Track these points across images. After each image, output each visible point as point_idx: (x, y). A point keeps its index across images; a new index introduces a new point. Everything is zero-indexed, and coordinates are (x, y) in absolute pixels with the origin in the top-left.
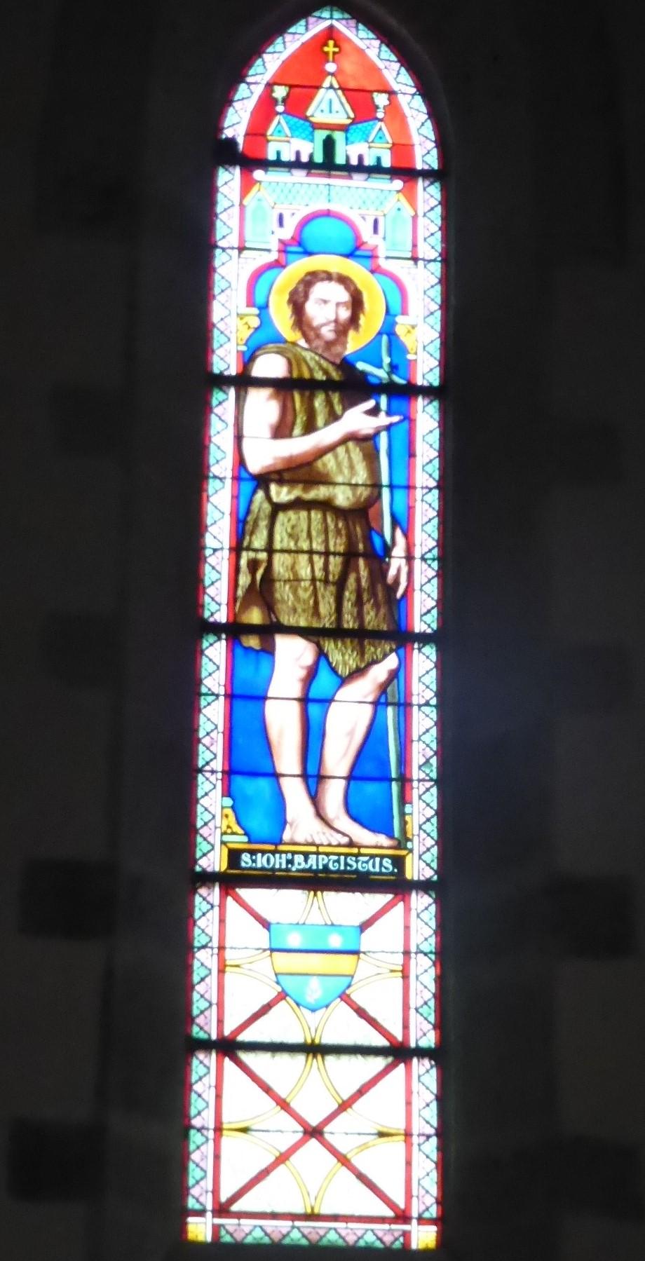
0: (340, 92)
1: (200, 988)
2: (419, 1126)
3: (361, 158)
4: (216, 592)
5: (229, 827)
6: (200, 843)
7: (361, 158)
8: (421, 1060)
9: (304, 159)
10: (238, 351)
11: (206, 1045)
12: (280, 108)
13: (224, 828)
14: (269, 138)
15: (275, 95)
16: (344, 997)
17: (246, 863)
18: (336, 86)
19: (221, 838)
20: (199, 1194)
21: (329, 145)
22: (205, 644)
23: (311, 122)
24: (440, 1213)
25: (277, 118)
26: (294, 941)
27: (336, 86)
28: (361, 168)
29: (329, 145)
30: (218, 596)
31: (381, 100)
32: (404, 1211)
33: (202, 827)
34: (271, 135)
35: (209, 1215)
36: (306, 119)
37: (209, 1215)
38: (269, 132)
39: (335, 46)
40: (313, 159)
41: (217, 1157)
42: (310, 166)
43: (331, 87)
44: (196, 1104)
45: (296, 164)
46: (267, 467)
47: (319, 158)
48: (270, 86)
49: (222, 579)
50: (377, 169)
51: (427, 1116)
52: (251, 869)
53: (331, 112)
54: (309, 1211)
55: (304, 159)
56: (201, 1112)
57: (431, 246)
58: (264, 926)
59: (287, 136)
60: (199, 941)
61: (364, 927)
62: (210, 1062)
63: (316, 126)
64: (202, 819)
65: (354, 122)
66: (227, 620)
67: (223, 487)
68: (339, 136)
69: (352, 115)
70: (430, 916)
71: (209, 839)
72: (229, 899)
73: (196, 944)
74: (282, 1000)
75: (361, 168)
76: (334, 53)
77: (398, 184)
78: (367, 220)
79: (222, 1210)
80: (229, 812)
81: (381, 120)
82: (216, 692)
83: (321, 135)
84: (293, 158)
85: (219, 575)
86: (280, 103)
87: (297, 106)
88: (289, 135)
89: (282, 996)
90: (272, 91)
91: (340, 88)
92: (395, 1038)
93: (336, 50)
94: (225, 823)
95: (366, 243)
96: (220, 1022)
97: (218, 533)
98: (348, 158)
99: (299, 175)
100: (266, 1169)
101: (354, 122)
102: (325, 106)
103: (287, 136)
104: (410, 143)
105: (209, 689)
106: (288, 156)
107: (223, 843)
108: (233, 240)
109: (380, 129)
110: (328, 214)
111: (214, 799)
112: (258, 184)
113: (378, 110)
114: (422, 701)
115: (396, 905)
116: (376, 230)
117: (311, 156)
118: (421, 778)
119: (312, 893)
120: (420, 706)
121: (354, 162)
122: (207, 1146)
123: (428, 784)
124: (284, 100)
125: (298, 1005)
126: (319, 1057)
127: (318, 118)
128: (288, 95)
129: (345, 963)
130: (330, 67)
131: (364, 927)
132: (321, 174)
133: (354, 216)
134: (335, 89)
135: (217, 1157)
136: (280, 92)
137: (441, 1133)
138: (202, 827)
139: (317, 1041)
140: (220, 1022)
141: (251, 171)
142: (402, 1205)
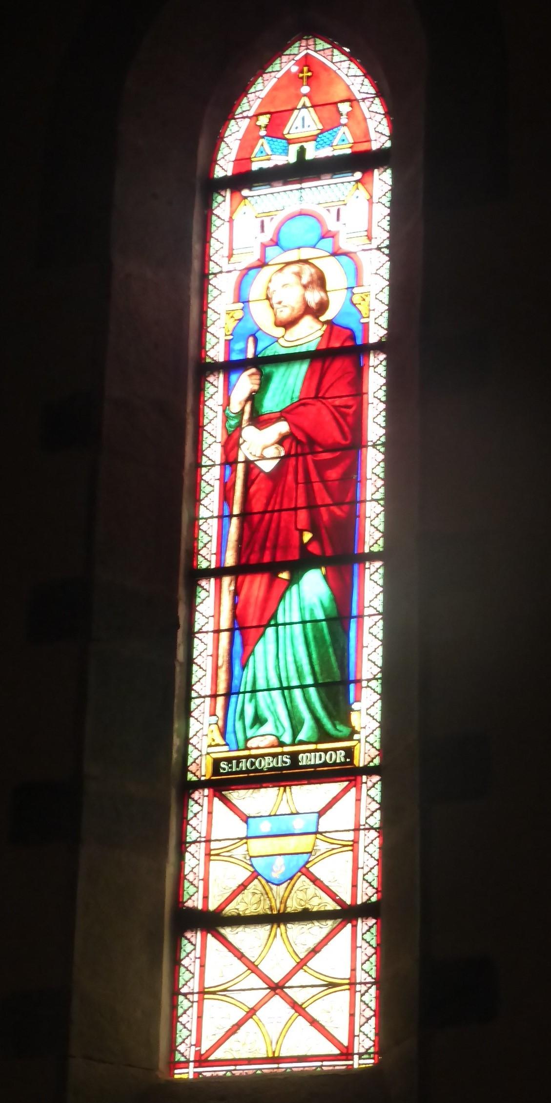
0: (311, 109)
2: (361, 976)
8: (364, 920)
10: (226, 340)
12: (263, 132)
14: (252, 159)
16: (304, 870)
17: (224, 769)
20: (186, 1050)
26: (265, 827)
27: (308, 104)
30: (189, 1023)
32: (347, 1048)
35: (192, 1065)
37: (192, 1065)
39: (309, 71)
41: (200, 1017)
43: (304, 106)
46: (252, 263)
49: (213, 540)
51: (367, 970)
52: (228, 773)
53: (303, 126)
54: (271, 1055)
56: (188, 982)
57: (382, 236)
59: (268, 155)
60: (190, 838)
61: (321, 813)
62: (210, 587)
63: (290, 142)
67: (224, 201)
70: (376, 793)
73: (188, 840)
74: (249, 1018)
76: (308, 77)
78: (331, 211)
79: (202, 1060)
81: (345, 125)
85: (220, 268)
87: (275, 129)
88: (270, 153)
89: (255, 875)
92: (345, 902)
93: (310, 74)
95: (330, 231)
96: (206, 898)
97: (213, 452)
100: (242, 884)
102: (299, 122)
103: (268, 155)
108: (194, 986)
113: (342, 117)
114: (362, 1050)
119: (275, 926)
122: (193, 1009)
125: (268, 881)
126: (282, 927)
129: (304, 843)
131: (321, 813)
132: (294, 180)
133: (320, 211)
135: (200, 1017)
136: (264, 120)
139: (282, 789)
140: (206, 898)
142: (346, 1043)
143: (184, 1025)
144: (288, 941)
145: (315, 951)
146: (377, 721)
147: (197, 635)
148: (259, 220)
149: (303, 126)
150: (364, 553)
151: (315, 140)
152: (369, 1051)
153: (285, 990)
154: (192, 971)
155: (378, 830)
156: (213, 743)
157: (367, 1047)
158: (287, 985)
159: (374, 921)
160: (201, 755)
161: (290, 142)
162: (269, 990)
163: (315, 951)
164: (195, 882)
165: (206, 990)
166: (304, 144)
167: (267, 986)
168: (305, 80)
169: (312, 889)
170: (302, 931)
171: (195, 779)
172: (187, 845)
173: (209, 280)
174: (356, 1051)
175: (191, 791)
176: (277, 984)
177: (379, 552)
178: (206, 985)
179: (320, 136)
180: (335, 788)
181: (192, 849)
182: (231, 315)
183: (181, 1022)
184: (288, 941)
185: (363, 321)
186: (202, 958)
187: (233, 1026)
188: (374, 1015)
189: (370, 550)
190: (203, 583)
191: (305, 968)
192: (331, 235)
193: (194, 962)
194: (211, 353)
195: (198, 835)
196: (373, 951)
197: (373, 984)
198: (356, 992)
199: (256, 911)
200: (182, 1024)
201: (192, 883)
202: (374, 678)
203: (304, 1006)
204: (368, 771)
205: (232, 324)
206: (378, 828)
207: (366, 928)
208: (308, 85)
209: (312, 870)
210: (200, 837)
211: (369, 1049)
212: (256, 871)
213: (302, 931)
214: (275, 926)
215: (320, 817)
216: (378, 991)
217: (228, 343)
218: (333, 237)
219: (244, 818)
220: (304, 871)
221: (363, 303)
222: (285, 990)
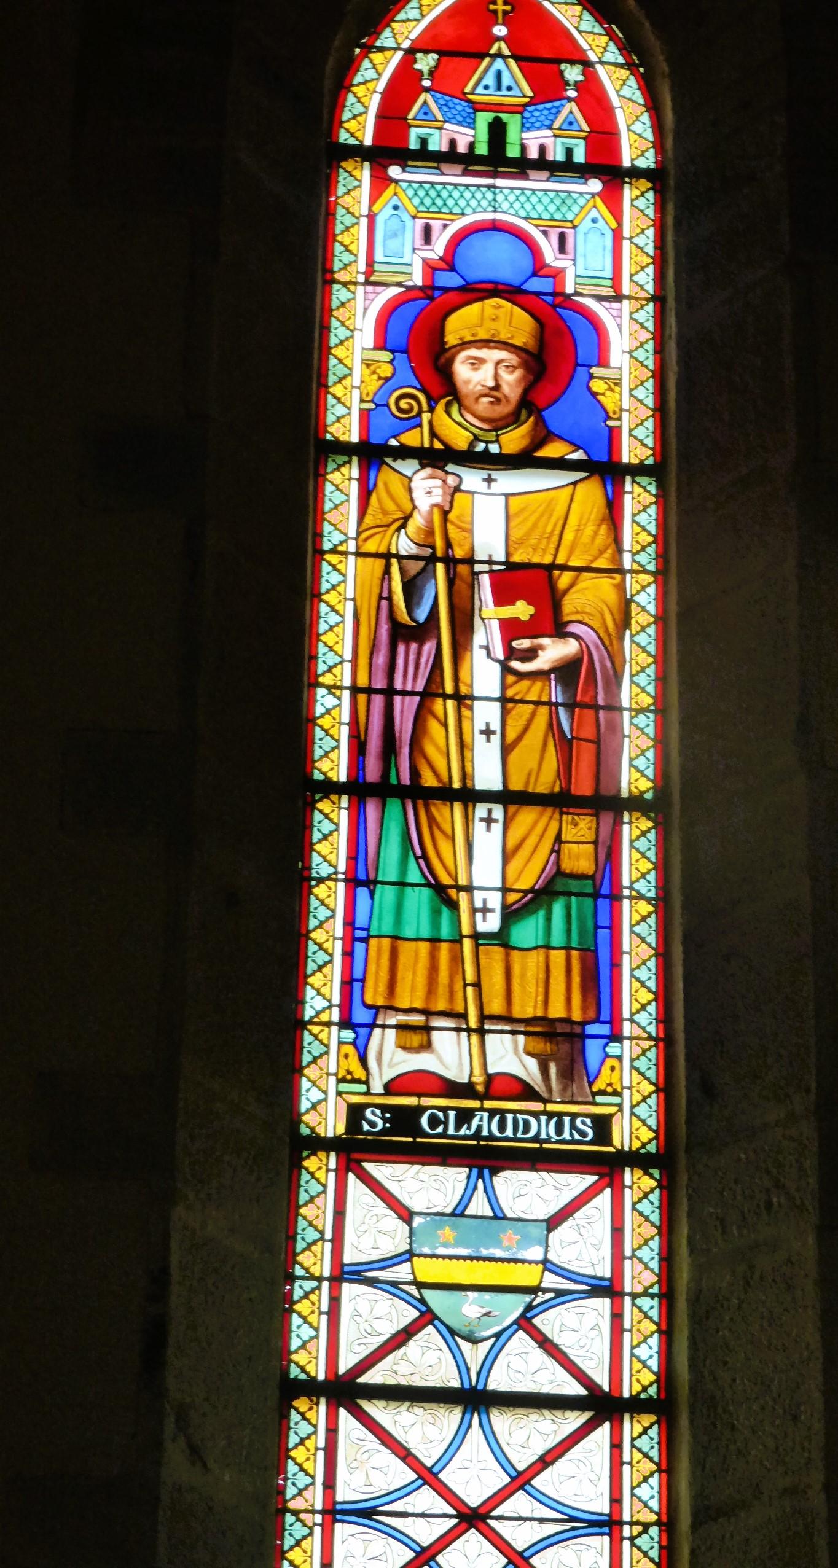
0: (511, 61)
1: (316, 980)
3: (542, 149)
4: (335, 639)
5: (349, 1072)
6: (336, 329)
7: (542, 149)
8: (635, 1415)
9: (462, 149)
10: (360, 409)
11: (311, 1388)
13: (341, 1075)
15: (417, 66)
17: (372, 1124)
18: (507, 52)
19: (337, 1087)
21: (497, 131)
22: (331, 466)
23: (469, 101)
24: (660, 610)
25: (423, 96)
28: (544, 164)
29: (497, 131)
31: (573, 73)
33: (337, 346)
34: (414, 119)
36: (463, 96)
38: (410, 116)
40: (462, 807)
42: (468, 161)
43: (499, 55)
44: (294, 1478)
45: (450, 157)
47: (482, 149)
48: (411, 52)
49: (363, 187)
50: (567, 168)
53: (499, 88)
55: (462, 149)
58: (401, 1218)
61: (554, 1222)
63: (477, 107)
64: (312, 1007)
65: (533, 102)
66: (326, 1377)
68: (513, 123)
69: (530, 94)
71: (336, 648)
72: (351, 1177)
75: (544, 164)
76: (505, 13)
77: (595, 185)
80: (350, 1049)
82: (317, 1274)
83: (484, 119)
84: (445, 148)
86: (426, 76)
88: (440, 118)
90: (415, 61)
91: (517, 58)
92: (600, 1388)
94: (344, 1064)
98: (523, 148)
99: (453, 176)
101: (533, 102)
102: (490, 80)
103: (437, 121)
104: (618, 705)
105: (307, 1270)
106: (437, 143)
107: (339, 1094)
109: (571, 112)
110: (495, 227)
111: (314, 1354)
112: (393, 185)
114: (639, 1289)
115: (601, 1191)
116: (562, 248)
117: (472, 146)
118: (634, 1035)
120: (634, 1296)
121: (533, 154)
123: (647, 1044)
124: (432, 73)
127: (480, 96)
128: (437, 66)
130: (500, 30)
131: (554, 1222)
134: (504, 57)
136: (425, 63)
137: (660, 708)
138: (337, 346)
141: (386, 167)
143: (312, 1174)
144: (491, 1438)
145: (545, 1461)
146: (649, 218)
147: (328, 557)
148: (420, 223)
149: (499, 88)
150: (621, 1398)
151: (521, 113)
152: (651, 1291)
153: (490, 1522)
154: (311, 1472)
155: (654, 902)
156: (349, 1077)
157: (647, 1284)
158: (494, 1513)
159: (653, 1418)
160: (341, 663)
161: (477, 107)
162: (455, 1521)
163: (545, 1461)
164: (313, 1319)
165: (338, 1507)
166: (500, 115)
167: (454, 1512)
168: (500, 15)
169: (538, 1356)
170: (521, 1425)
171: (352, 141)
172: (313, 883)
173: (311, 887)
174: (627, 1288)
175: (305, 1154)
176: (474, 1510)
177: (648, 169)
178: (339, 1498)
179: (529, 108)
180: (580, 1182)
181: (321, 891)
182: (372, 368)
183: (312, 986)
184: (491, 1438)
185: (610, 423)
186: (331, 1450)
187: (398, 1333)
188: (653, 263)
189: (632, 164)
190: (324, 806)
191: (527, 1487)
192: (552, 274)
193: (315, 1455)
194: (325, 765)
195: (332, 870)
196: (651, 996)
197: (648, 300)
198: (622, 1539)
199: (428, 1378)
200: (323, 730)
201: (320, 947)
202: (645, 1293)
203: (526, 1554)
204: (638, 1160)
205: (373, 385)
206: (653, 899)
207: (638, 1429)
208: (504, 24)
209: (536, 1321)
210: (336, 873)
211: (651, 1286)
212: (429, 1310)
213: (521, 1425)
214: (469, 1409)
215: (550, 1229)
216: (658, 356)
217: (365, 415)
218: (554, 277)
219: (405, 1214)
220: (525, 1323)
221: (608, 393)
222: (490, 1522)
